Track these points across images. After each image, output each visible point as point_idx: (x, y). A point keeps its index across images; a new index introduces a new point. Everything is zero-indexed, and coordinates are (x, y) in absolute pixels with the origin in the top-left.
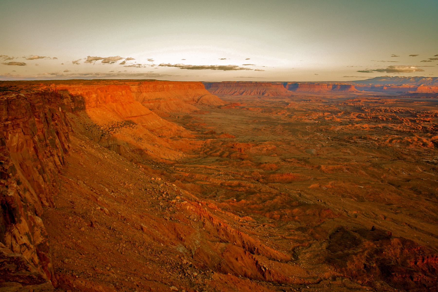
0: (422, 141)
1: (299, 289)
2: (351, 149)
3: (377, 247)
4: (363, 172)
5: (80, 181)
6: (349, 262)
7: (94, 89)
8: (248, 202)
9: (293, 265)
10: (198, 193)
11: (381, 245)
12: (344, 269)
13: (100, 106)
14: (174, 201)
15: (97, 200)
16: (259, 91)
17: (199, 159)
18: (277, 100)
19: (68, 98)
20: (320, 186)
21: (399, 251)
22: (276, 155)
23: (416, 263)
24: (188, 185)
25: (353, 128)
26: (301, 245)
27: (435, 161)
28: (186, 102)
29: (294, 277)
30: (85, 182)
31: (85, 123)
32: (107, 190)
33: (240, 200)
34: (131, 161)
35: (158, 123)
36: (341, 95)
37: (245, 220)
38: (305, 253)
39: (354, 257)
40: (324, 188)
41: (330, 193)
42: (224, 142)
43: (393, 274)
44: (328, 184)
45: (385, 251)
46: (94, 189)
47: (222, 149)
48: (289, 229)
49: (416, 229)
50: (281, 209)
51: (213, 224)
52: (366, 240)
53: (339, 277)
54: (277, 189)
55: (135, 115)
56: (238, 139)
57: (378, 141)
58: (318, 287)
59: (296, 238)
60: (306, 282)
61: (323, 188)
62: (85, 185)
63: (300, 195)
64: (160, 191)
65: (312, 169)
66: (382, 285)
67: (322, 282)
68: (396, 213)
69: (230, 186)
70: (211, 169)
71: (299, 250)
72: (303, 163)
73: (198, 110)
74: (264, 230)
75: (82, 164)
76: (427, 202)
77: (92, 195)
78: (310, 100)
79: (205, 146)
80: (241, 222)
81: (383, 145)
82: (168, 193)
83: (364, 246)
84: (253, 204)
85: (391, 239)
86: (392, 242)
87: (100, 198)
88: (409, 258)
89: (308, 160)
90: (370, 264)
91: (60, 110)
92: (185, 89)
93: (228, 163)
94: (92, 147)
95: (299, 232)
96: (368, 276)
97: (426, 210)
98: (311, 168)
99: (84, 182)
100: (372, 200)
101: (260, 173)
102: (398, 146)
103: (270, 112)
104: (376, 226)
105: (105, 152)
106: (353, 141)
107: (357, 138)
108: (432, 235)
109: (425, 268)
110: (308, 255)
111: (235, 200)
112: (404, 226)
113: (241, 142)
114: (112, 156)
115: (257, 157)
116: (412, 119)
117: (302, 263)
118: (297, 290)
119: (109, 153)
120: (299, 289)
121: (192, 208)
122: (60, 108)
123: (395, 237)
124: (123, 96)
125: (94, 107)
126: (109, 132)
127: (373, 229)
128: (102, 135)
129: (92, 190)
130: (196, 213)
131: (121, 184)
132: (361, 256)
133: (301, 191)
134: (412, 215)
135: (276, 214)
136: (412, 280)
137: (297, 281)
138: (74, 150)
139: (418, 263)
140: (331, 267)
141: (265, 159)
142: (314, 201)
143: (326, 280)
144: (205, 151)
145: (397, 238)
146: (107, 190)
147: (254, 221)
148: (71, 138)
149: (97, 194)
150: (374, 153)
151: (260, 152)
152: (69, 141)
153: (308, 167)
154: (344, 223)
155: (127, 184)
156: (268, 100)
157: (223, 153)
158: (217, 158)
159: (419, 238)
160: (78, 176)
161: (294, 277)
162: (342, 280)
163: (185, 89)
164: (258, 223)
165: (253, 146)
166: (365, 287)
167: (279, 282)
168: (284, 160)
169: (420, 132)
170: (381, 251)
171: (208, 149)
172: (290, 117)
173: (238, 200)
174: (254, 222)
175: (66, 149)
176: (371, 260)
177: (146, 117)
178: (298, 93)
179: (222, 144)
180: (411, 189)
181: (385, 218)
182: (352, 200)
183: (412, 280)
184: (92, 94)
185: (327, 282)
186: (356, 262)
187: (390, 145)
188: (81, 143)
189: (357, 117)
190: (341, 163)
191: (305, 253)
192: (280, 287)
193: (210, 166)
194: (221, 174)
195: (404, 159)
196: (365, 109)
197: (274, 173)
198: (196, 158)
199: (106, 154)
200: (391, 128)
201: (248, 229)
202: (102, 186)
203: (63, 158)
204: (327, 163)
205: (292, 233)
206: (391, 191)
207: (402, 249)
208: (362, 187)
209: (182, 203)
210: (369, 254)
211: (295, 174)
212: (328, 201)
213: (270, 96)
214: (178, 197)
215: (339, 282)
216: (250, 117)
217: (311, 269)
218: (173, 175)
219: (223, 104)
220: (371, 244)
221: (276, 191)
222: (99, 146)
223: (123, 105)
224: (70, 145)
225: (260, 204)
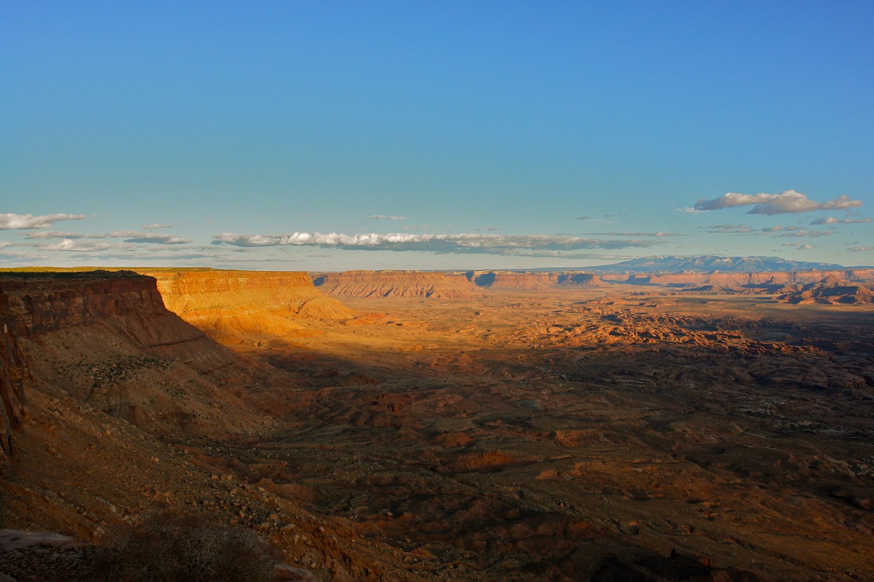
4: (636, 440)
5: (51, 492)
7: (79, 285)
8: (418, 518)
10: (310, 504)
13: (91, 322)
14: (266, 525)
15: (91, 533)
16: (420, 289)
17: (308, 430)
18: (457, 306)
19: (19, 305)
20: (558, 474)
22: (464, 415)
24: (288, 487)
25: (607, 355)
27: (760, 410)
28: (273, 312)
30: (62, 494)
31: (55, 358)
32: (114, 509)
33: (401, 514)
34: (161, 439)
35: (217, 356)
36: (577, 293)
37: (417, 557)
40: (567, 477)
42: (358, 393)
46: (85, 510)
47: (354, 408)
48: (508, 570)
50: (486, 528)
51: (351, 571)
54: (474, 485)
55: (169, 340)
56: (385, 384)
57: (654, 377)
62: (62, 500)
63: (521, 494)
64: (232, 504)
65: (539, 440)
69: (377, 485)
70: (333, 450)
72: (520, 429)
73: (300, 328)
74: (458, 577)
75: (54, 450)
76: (763, 491)
77: (80, 525)
78: (519, 305)
79: (318, 402)
80: (408, 562)
82: (252, 506)
84: (428, 521)
87: (99, 529)
89: (528, 422)
91: (6, 331)
92: (271, 287)
93: (368, 435)
94: (77, 411)
98: (536, 438)
99: (59, 495)
101: (438, 454)
102: (692, 385)
103: (445, 328)
105: (106, 423)
107: (616, 374)
111: (390, 514)
112: (730, 543)
113: (392, 391)
114: (120, 430)
115: (426, 420)
116: (710, 333)
119: (114, 425)
121: (304, 538)
122: (5, 327)
123: (719, 569)
124: (142, 300)
125: (77, 325)
126: (110, 377)
127: (674, 555)
128: (95, 386)
129: (79, 512)
130: (314, 550)
131: (146, 494)
133: (522, 486)
135: (478, 538)
138: (34, 419)
141: (443, 425)
142: (550, 505)
144: (319, 413)
145: (724, 569)
146: (114, 509)
147: (434, 557)
148: (28, 392)
149: (91, 519)
151: (431, 410)
152: (22, 400)
153: (530, 437)
155: (158, 493)
156: (438, 307)
157: (357, 415)
158: (346, 426)
160: (46, 481)
163: (271, 287)
164: (441, 560)
165: (417, 399)
168: (480, 424)
169: (727, 358)
171: (326, 409)
172: (486, 337)
173: (397, 515)
174: (433, 561)
175: (16, 418)
177: (189, 343)
178: (495, 291)
179: (354, 398)
180: (729, 468)
184: (74, 296)
187: (677, 384)
188: (52, 403)
189: (611, 333)
190: (594, 425)
193: (332, 443)
194: (357, 461)
195: (708, 410)
196: (624, 317)
197: (464, 452)
198: (301, 429)
199: (108, 426)
200: (675, 352)
201: (423, 576)
202: (102, 501)
203: (9, 439)
204: (566, 426)
205: (516, 577)
206: (695, 475)
208: (640, 470)
209: (283, 528)
211: (507, 452)
213: (441, 298)
214: (274, 516)
216: (405, 340)
218: (253, 468)
219: (350, 317)
221: (473, 489)
222: (91, 409)
223: (142, 320)
224: (26, 409)
225: (442, 519)
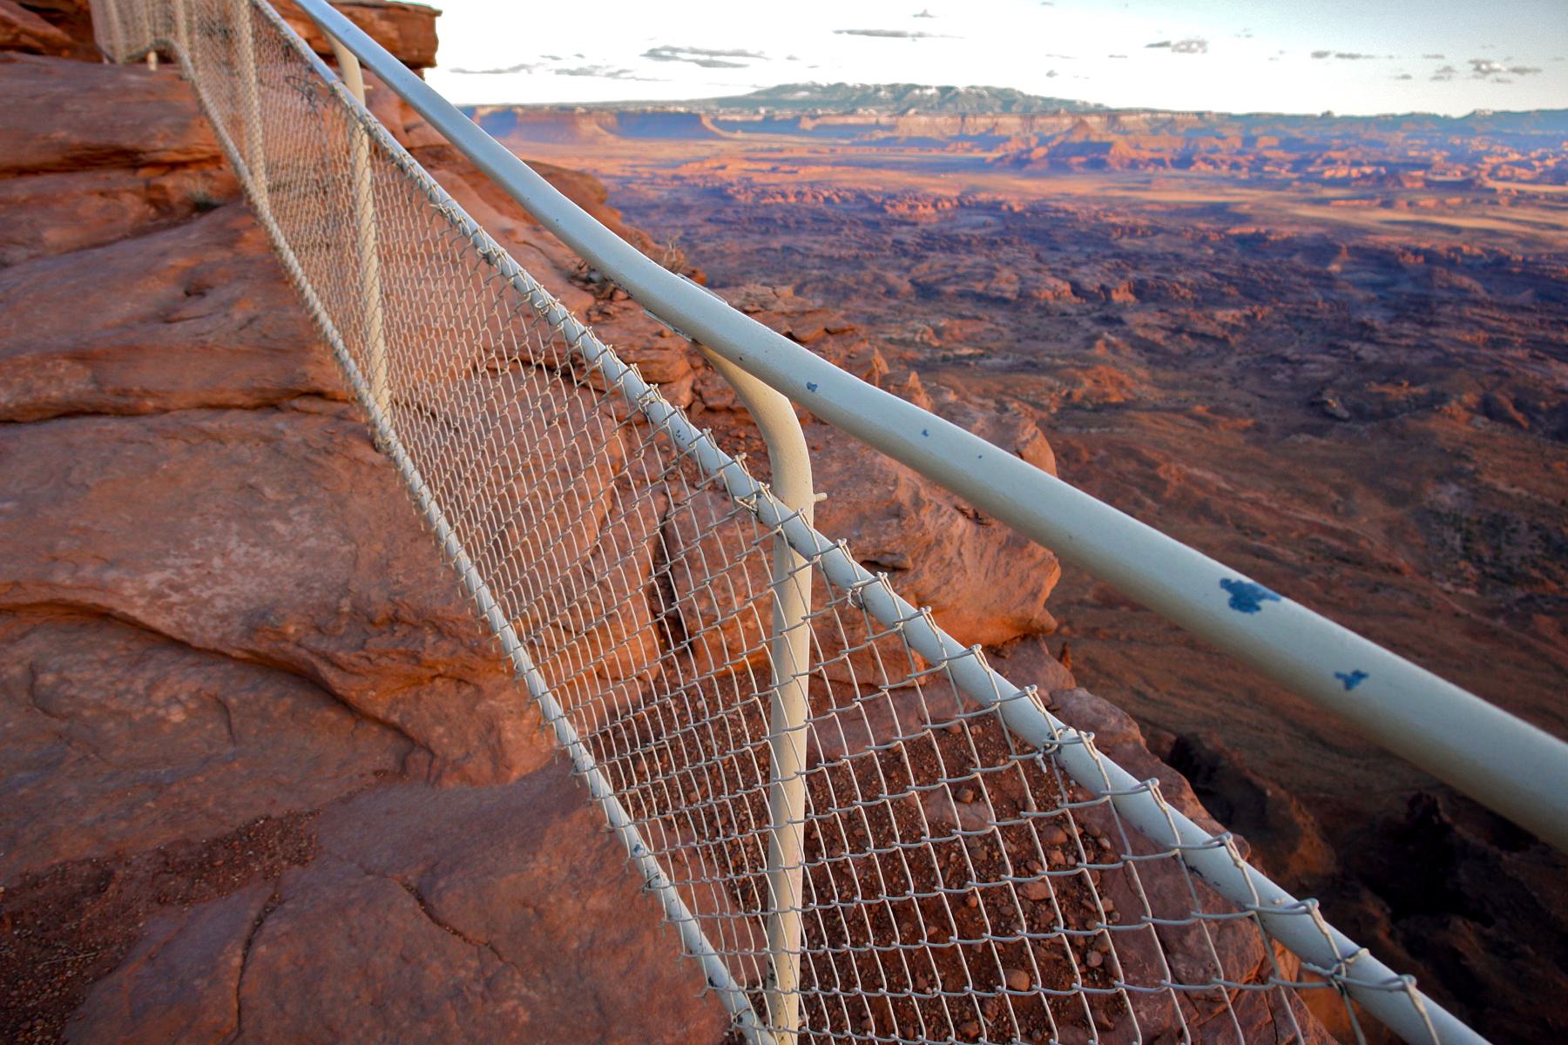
0: (884, 283)
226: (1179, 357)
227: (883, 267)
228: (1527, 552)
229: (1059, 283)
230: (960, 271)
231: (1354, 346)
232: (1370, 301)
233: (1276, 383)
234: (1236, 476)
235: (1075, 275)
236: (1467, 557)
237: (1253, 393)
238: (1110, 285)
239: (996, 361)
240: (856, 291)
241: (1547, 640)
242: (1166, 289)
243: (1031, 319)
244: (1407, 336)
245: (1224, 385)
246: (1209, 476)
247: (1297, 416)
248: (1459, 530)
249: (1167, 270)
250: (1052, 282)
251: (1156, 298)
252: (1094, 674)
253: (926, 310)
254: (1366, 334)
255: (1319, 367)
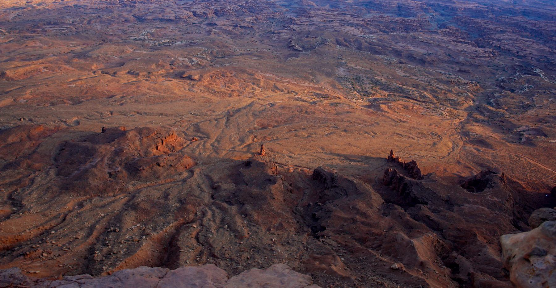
0: (123, 17)
1: (42, 240)
2: (41, 42)
3: (116, 148)
6: (91, 178)
9: (20, 217)
11: (119, 144)
12: (88, 189)
20: (14, 100)
21: (138, 143)
23: (157, 148)
26: (19, 186)
27: (141, 37)
29: (28, 231)
38: (30, 194)
39: (94, 170)
41: (34, 105)
43: (141, 168)
44: (26, 94)
45: (125, 149)
49: (146, 113)
52: (100, 145)
53: (86, 200)
57: (73, 24)
58: (65, 226)
59: (8, 180)
60: (47, 227)
61: (20, 101)
66: (134, 185)
67: (68, 216)
68: (122, 104)
71: (19, 193)
81: (81, 29)
83: (101, 153)
85: (127, 134)
86: (129, 136)
88: (150, 146)
90: (115, 169)
95: (10, 171)
96: (117, 183)
97: (149, 91)
100: (90, 98)
102: (99, 27)
104: (106, 126)
106: (41, 30)
107: (44, 24)
108: (162, 114)
109: (166, 150)
110: (35, 195)
117: (31, 208)
118: (40, 244)
120: (42, 240)
127: (104, 130)
132: (101, 165)
134: (138, 101)
136: (159, 165)
137: (34, 232)
139: (159, 148)
140: (72, 194)
142: (13, 122)
143: (72, 211)
150: (73, 40)
154: (66, 137)
159: (151, 122)
161: (28, 231)
162: (91, 202)
166: (118, 197)
167: (8, 249)
170: (121, 150)
176: (114, 165)
181: (112, 114)
182: (66, 105)
183: (159, 165)
185: (74, 213)
186: (99, 175)
187: (89, 27)
191: (30, 194)
192: (15, 253)
195: (111, 41)
200: (85, 6)
207: (141, 139)
208: (73, 86)
210: (110, 159)
212: (35, 116)
215: (88, 206)
217: (46, 209)
220: (108, 147)
226: (240, 35)
227: (121, 11)
228: (368, 86)
229: (189, 12)
230: (151, 11)
231: (292, 26)
232: (287, 11)
233: (274, 41)
234: (279, 74)
235: (192, 9)
236: (354, 90)
237: (269, 45)
238: (206, 12)
239: (179, 43)
240: (113, 21)
241: (386, 112)
242: (225, 12)
243: (183, 26)
244: (306, 22)
245: (258, 43)
246: (271, 76)
247: (287, 52)
248: (349, 82)
249: (223, 5)
250: (186, 12)
251: (223, 15)
252: (273, 153)
253: (143, 27)
254: (293, 22)
255: (285, 34)
